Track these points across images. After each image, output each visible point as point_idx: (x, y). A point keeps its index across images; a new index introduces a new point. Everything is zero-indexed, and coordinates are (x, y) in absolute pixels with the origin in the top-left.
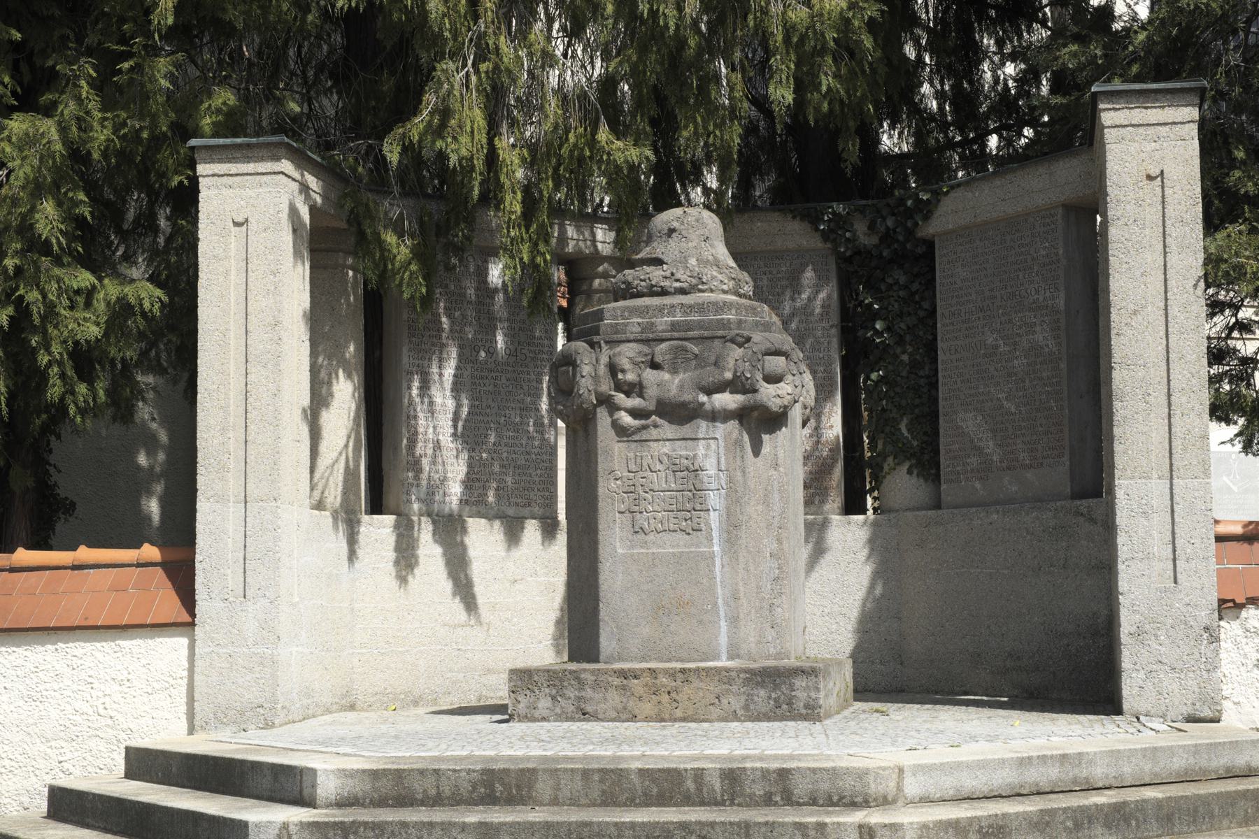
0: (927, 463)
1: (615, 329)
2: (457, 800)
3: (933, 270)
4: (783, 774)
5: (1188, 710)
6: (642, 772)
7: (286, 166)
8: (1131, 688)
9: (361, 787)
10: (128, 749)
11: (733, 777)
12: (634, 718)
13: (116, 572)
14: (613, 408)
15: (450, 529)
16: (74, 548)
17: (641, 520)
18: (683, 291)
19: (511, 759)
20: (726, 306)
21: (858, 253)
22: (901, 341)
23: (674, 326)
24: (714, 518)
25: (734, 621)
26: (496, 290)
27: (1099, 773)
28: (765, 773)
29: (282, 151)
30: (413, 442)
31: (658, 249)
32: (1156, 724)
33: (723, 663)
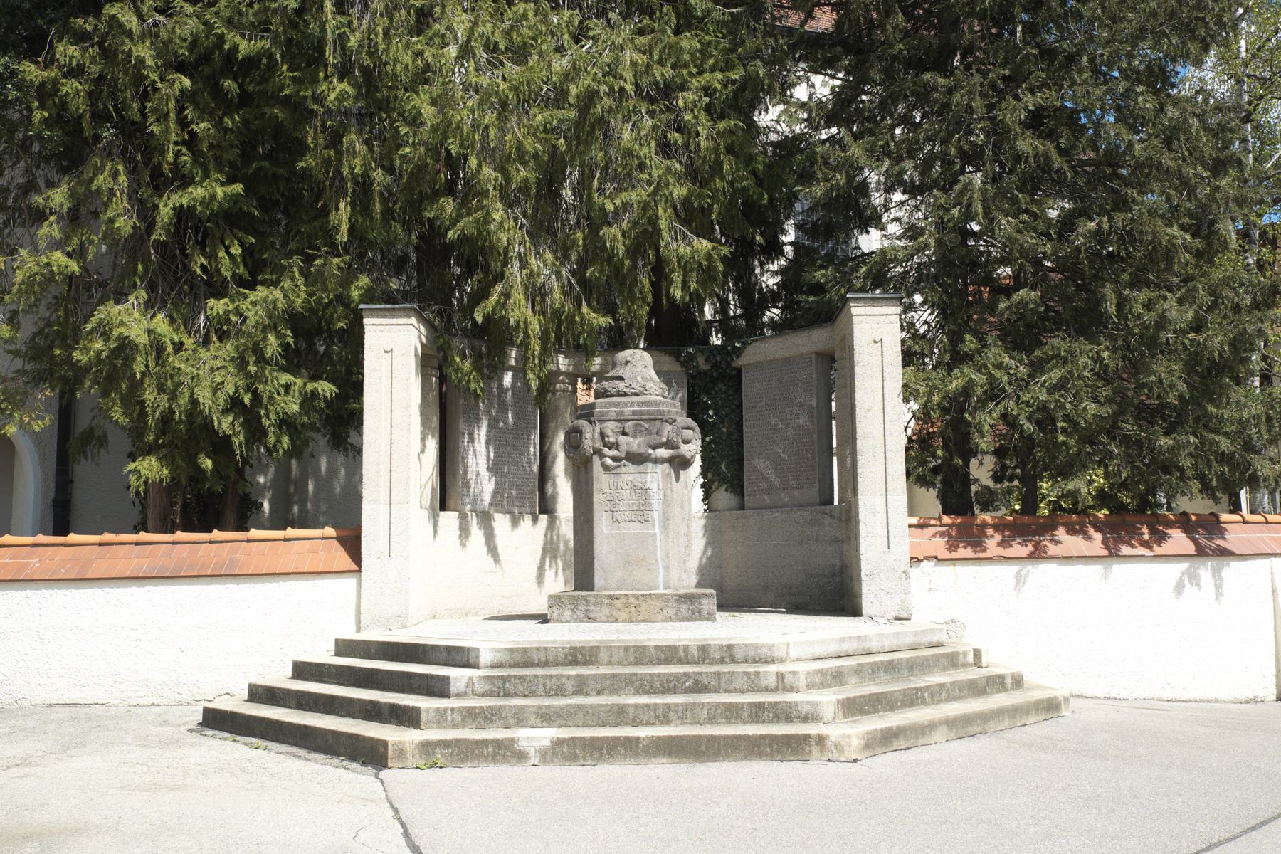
0: (737, 486)
1: (603, 414)
2: (557, 664)
3: (740, 383)
4: (730, 647)
5: (895, 614)
6: (656, 647)
7: (413, 320)
8: (867, 603)
9: (504, 657)
10: (337, 641)
11: (704, 649)
12: (616, 620)
13: (316, 543)
14: (602, 456)
15: (485, 519)
16: (173, 533)
17: (617, 515)
18: (636, 394)
19: (580, 642)
20: (657, 404)
21: (699, 373)
22: (722, 421)
23: (634, 413)
24: (656, 515)
25: (667, 569)
26: (508, 389)
27: (874, 645)
28: (721, 647)
29: (412, 313)
30: (466, 472)
31: (620, 371)
32: (881, 620)
33: (661, 591)
